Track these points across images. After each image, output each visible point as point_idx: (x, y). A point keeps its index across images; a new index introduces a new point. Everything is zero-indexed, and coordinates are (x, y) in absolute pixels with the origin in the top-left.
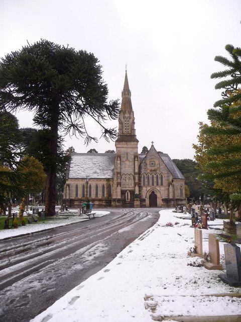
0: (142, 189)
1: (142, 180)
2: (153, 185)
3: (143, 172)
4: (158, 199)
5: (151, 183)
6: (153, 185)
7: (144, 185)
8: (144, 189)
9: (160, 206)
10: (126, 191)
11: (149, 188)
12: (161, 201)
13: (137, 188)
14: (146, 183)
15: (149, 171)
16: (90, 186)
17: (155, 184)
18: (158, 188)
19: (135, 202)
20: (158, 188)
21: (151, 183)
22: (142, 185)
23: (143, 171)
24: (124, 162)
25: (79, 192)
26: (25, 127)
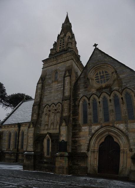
0: (80, 130)
1: (81, 110)
2: (107, 119)
3: (81, 95)
4: (121, 155)
5: (101, 116)
6: (107, 119)
7: (85, 122)
8: (85, 129)
9: (126, 173)
10: (44, 136)
11: (97, 127)
12: (129, 161)
13: (64, 130)
14: (90, 117)
15: (94, 91)
16: (23, 133)
17: (112, 118)
18: (122, 126)
19: (59, 159)
20: (122, 126)
21: (101, 116)
22: (81, 120)
23: (81, 92)
24: (49, 85)
25: (19, 143)
26: (10, 94)
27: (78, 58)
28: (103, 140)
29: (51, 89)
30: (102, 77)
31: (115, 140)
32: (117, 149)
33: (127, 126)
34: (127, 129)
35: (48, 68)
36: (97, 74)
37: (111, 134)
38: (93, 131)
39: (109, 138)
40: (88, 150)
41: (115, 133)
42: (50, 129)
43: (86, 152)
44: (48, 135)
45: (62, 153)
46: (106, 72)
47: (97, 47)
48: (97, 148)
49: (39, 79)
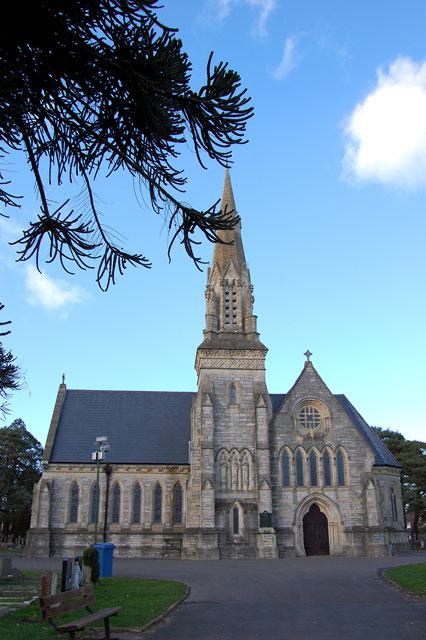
4: (330, 529)
6: (314, 482)
22: (280, 483)
27: (35, 442)
28: (307, 511)
29: (227, 420)
30: (310, 418)
31: (322, 510)
32: (322, 521)
33: (337, 494)
34: (337, 498)
35: (216, 371)
36: (303, 411)
37: (318, 502)
38: (299, 500)
39: (315, 508)
40: (294, 524)
41: (324, 502)
42: (231, 491)
43: (290, 526)
44: (237, 503)
45: (267, 529)
46: (316, 411)
47: (311, 358)
48: (301, 518)
49: (35, 437)
